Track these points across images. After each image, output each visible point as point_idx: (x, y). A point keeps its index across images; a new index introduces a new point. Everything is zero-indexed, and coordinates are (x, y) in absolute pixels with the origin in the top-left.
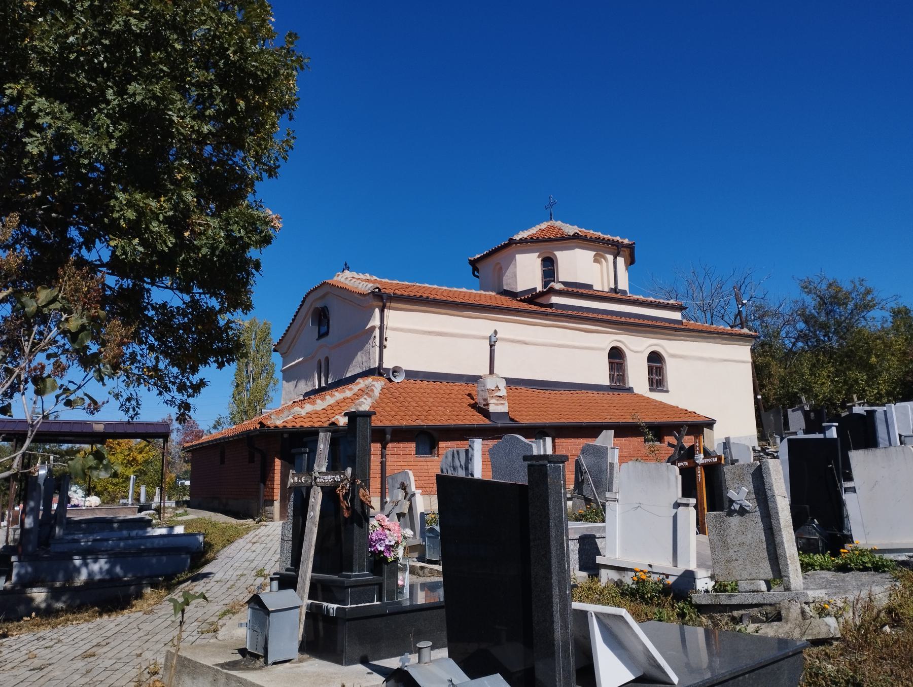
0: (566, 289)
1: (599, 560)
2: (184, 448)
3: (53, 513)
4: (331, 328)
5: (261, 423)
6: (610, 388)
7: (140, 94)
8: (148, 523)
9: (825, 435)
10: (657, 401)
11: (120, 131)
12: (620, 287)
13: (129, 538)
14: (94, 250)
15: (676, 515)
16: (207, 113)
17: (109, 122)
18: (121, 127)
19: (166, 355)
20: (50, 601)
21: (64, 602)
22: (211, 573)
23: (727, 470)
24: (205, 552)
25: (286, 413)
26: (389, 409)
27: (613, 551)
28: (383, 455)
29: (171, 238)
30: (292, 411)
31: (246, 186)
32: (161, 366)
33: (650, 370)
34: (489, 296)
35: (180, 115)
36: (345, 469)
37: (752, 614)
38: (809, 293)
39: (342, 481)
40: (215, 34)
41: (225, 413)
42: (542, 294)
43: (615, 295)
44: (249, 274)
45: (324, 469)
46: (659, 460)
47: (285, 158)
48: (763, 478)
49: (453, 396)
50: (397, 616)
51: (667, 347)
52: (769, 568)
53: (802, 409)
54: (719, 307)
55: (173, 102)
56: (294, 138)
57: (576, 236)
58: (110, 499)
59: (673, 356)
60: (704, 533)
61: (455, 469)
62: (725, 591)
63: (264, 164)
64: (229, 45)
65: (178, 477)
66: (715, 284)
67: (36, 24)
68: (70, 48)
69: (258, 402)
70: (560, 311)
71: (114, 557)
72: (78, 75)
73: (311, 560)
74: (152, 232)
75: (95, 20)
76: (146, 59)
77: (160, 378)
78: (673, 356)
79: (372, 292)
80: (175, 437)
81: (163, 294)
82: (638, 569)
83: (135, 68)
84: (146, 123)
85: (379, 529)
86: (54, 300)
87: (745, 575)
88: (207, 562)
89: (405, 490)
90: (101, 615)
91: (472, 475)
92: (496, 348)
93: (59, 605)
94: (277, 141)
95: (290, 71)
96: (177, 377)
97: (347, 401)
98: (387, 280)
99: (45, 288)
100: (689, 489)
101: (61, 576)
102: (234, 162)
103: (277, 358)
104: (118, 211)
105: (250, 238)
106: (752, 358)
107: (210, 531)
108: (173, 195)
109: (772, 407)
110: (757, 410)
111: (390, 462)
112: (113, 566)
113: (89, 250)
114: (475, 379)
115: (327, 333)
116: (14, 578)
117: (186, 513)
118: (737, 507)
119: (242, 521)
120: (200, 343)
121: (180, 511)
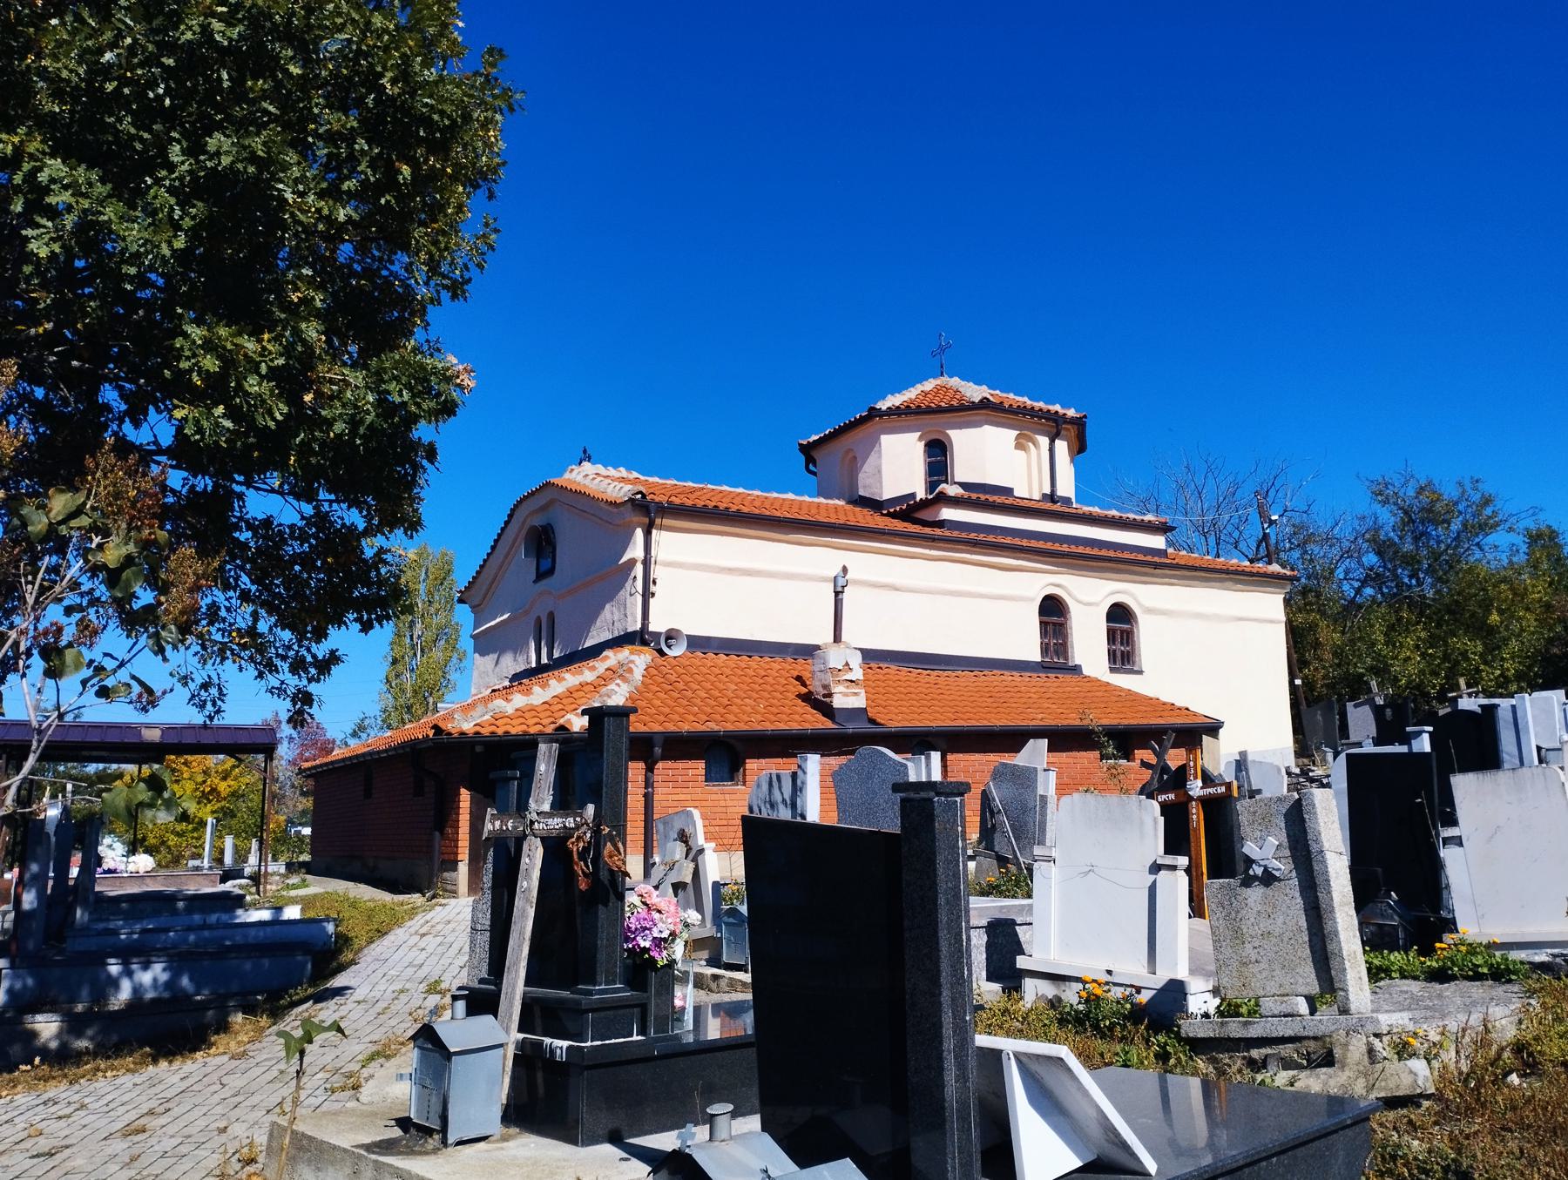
1: (1022, 962)
2: (301, 771)
3: (71, 883)
4: (558, 563)
5: (435, 727)
8: (237, 901)
10: (1121, 689)
11: (193, 218)
12: (1060, 492)
13: (205, 926)
14: (145, 425)
16: (345, 187)
17: (173, 201)
18: (193, 211)
20: (65, 1038)
21: (91, 1039)
23: (1243, 807)
24: (339, 951)
25: (480, 709)
27: (1043, 948)
28: (648, 783)
29: (281, 406)
30: (490, 706)
31: (413, 314)
32: (263, 627)
33: (1111, 636)
35: (298, 192)
36: (583, 806)
38: (1385, 502)
39: (578, 827)
40: (359, 48)
42: (925, 504)
43: (1052, 507)
44: (417, 467)
45: (546, 807)
46: (1125, 791)
47: (480, 266)
48: (1303, 821)
49: (770, 679)
51: (1140, 595)
52: (1313, 976)
53: (1371, 702)
54: (1230, 528)
55: (285, 167)
56: (496, 231)
57: (985, 404)
59: (1150, 611)
60: (1202, 916)
61: (773, 806)
62: (1238, 1015)
63: (444, 276)
64: (385, 68)
65: (290, 821)
66: (1223, 487)
67: (46, 29)
68: (106, 71)
69: (428, 692)
70: (956, 534)
71: (178, 960)
72: (120, 120)
74: (248, 394)
76: (239, 93)
77: (261, 649)
78: (1150, 611)
79: (630, 500)
80: (284, 751)
81: (266, 504)
82: (1089, 976)
84: (238, 204)
85: (642, 909)
86: (78, 512)
87: (1272, 988)
89: (686, 842)
90: (155, 1061)
91: (803, 817)
92: (847, 597)
93: (82, 1044)
94: (467, 236)
96: (289, 648)
97: (586, 689)
98: (656, 479)
99: (62, 491)
100: (1176, 840)
101: (85, 993)
102: (391, 273)
103: (463, 614)
104: (188, 358)
105: (418, 405)
106: (1287, 614)
107: (347, 915)
108: (284, 329)
109: (1318, 699)
113: (137, 424)
114: (808, 651)
115: (551, 572)
118: (1259, 871)
119: (401, 897)
120: (329, 588)
121: (295, 880)
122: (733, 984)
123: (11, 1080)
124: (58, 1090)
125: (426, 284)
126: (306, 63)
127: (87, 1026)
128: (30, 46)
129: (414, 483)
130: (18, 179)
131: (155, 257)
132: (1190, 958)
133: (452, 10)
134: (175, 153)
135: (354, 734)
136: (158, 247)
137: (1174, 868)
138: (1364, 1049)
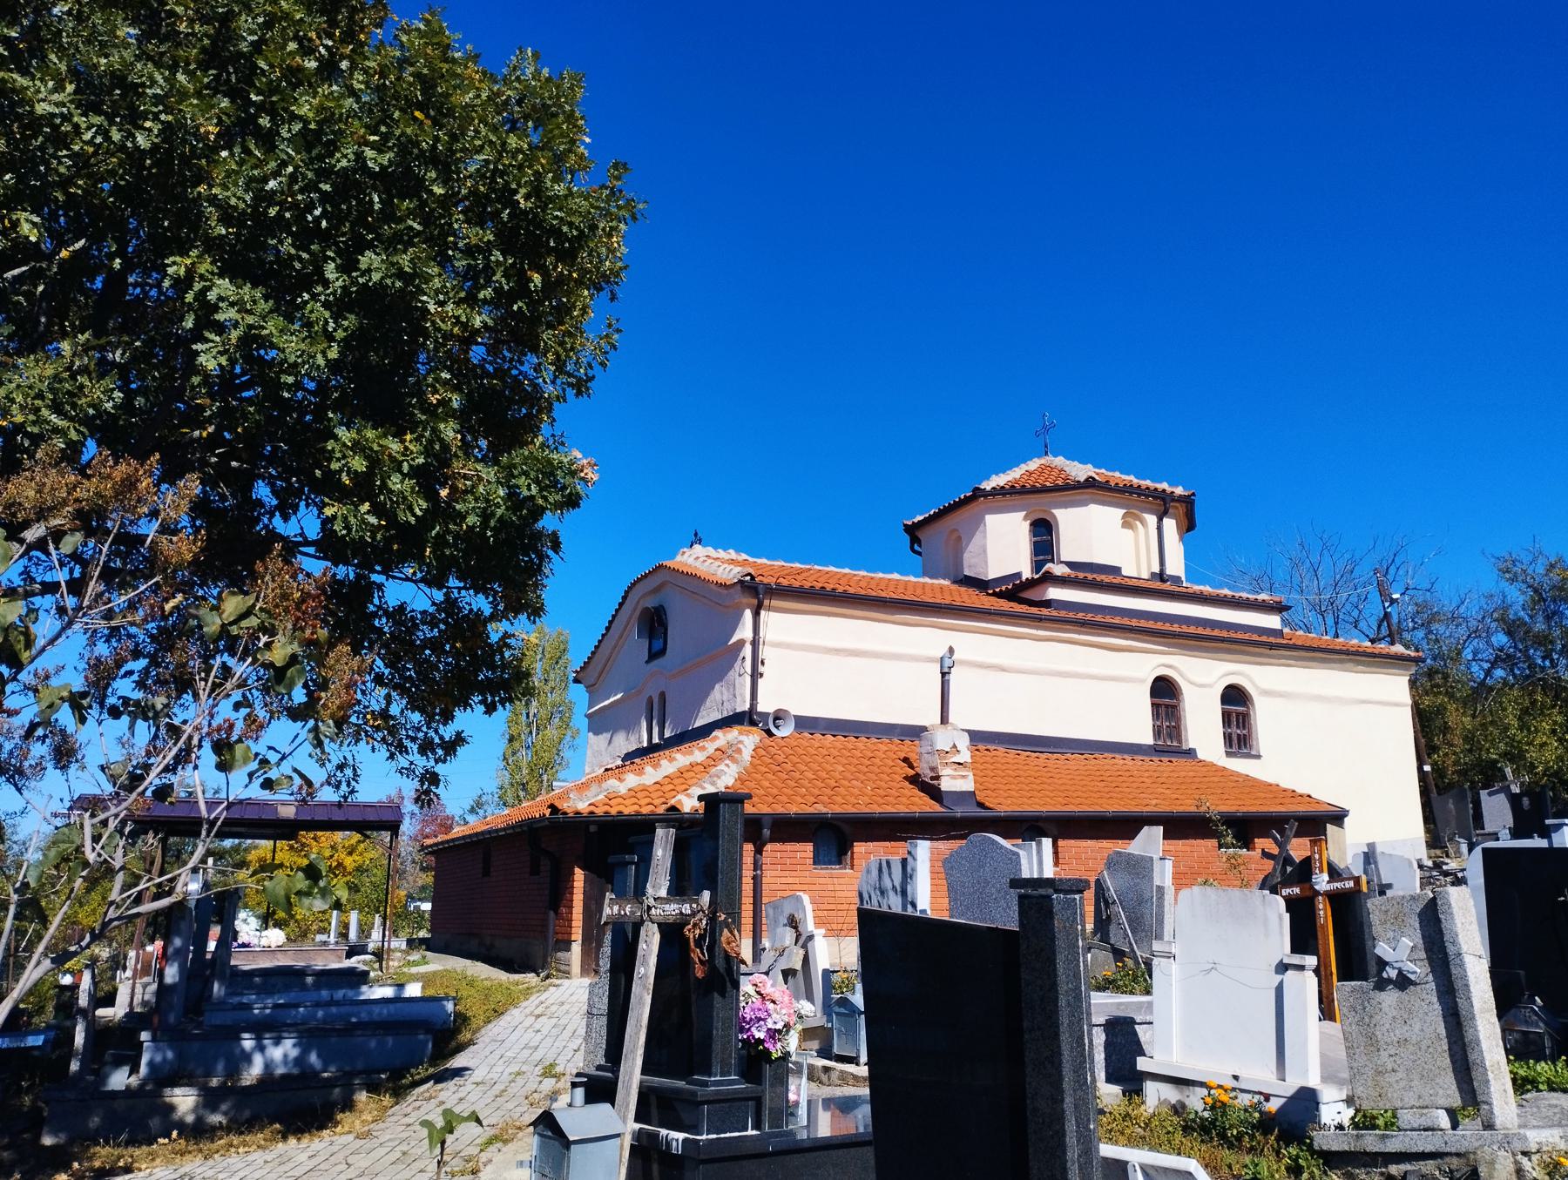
0: (1073, 574)
1: (1142, 1064)
2: (423, 848)
3: (209, 956)
4: (669, 644)
5: (552, 806)
6: (1155, 750)
7: (377, 269)
8: (360, 978)
9: (1550, 842)
10: (1239, 775)
11: (345, 330)
12: (1170, 571)
13: (332, 1002)
14: (293, 518)
15: (1281, 983)
16: (481, 296)
17: (327, 314)
18: (346, 323)
19: (403, 691)
20: (201, 1112)
21: (225, 1114)
22: (467, 1069)
23: (1374, 905)
24: (457, 1031)
25: (594, 788)
26: (767, 784)
27: (1164, 1050)
28: (757, 866)
29: (421, 502)
30: (604, 785)
31: (540, 411)
32: (395, 710)
33: (1227, 718)
34: (939, 587)
35: (441, 305)
36: (699, 893)
37: (1424, 1170)
38: (1513, 580)
39: (694, 914)
40: (496, 168)
41: (491, 786)
42: (1031, 583)
43: (1161, 586)
44: (542, 557)
45: (663, 893)
46: (1245, 885)
47: (603, 364)
48: (1439, 921)
49: (877, 761)
50: (788, 1158)
51: (1255, 676)
52: (1454, 1087)
53: (1506, 790)
54: (1348, 607)
55: (428, 279)
56: (618, 331)
57: (1090, 483)
58: (300, 935)
59: (1266, 693)
60: (1332, 1018)
61: (883, 892)
62: (1374, 1127)
63: (570, 375)
64: (519, 185)
65: (410, 897)
66: (1340, 565)
67: (217, 162)
68: (270, 198)
69: (544, 768)
70: (1063, 614)
71: (309, 1036)
72: (281, 242)
73: (640, 1051)
74: (391, 491)
75: (309, 152)
76: (388, 214)
77: (393, 731)
78: (1266, 693)
79: (740, 582)
80: (407, 828)
81: (404, 592)
82: (1214, 1082)
83: (370, 228)
84: (386, 317)
85: (756, 999)
86: (247, 613)
87: (1411, 1099)
88: (461, 1048)
89: (796, 928)
90: (285, 1138)
91: (914, 905)
92: (953, 678)
93: (216, 1118)
94: (591, 336)
95: (614, 224)
96: (419, 729)
98: (764, 561)
99: (234, 594)
100: (1303, 939)
101: (220, 1067)
102: (521, 373)
103: (578, 694)
104: (338, 460)
105: (545, 498)
106: (1413, 697)
107: (465, 994)
108: (425, 429)
109: (1451, 786)
110: (1425, 792)
111: (769, 877)
112: (305, 1052)
113: (286, 519)
114: (916, 732)
115: (663, 652)
116: (143, 1070)
117: (424, 961)
118: (1393, 974)
119: (516, 977)
120: (460, 672)
121: (415, 956)
122: (844, 1078)
123: (150, 1154)
124: (193, 1164)
125: (553, 382)
126: (445, 180)
127: (223, 1100)
128: (202, 177)
129: (539, 570)
130: (189, 297)
131: (311, 367)
132: (1322, 1065)
133: (579, 128)
134: (330, 271)
135: (472, 811)
136: (314, 357)
137: (1301, 968)
138: (1512, 1168)
